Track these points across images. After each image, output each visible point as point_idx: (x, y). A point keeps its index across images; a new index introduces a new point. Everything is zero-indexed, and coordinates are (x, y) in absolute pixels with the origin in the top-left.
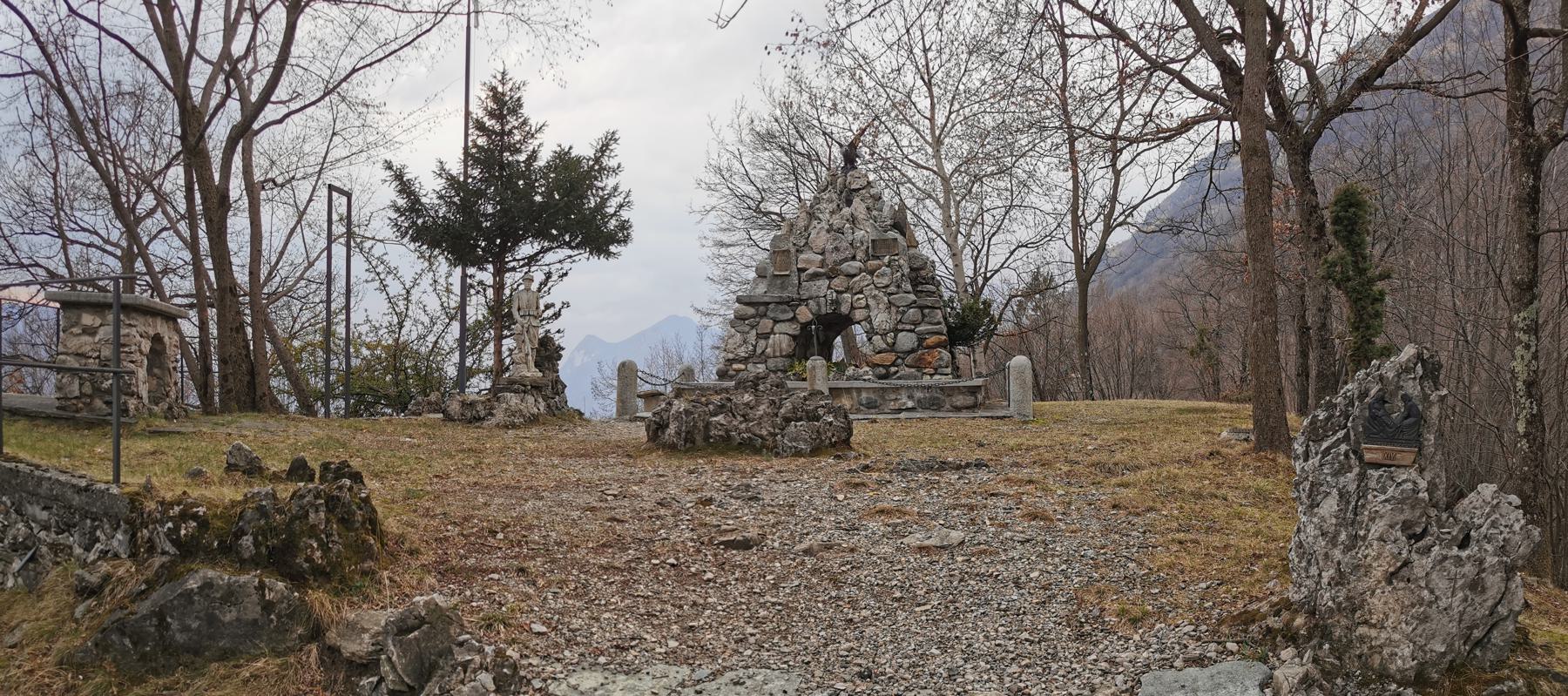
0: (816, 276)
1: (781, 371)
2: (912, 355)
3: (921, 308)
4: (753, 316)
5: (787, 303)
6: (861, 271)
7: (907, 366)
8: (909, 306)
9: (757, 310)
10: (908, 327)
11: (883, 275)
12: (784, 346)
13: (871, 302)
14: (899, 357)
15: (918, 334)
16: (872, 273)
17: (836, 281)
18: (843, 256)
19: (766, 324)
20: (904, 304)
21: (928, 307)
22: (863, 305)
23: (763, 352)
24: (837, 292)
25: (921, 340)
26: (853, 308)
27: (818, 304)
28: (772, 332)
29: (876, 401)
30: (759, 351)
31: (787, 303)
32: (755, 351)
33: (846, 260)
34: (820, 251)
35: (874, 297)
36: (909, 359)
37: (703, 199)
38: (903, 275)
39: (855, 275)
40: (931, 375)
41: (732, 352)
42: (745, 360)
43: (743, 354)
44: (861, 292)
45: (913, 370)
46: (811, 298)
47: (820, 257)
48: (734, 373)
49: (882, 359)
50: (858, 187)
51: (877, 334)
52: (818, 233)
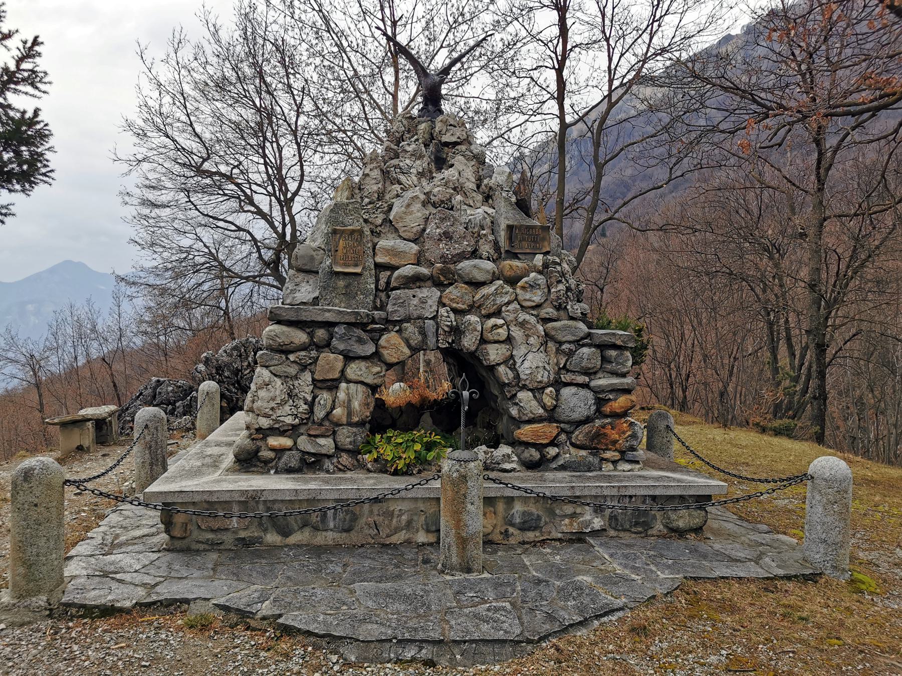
0: (415, 281)
1: (348, 451)
2: (586, 428)
3: (602, 347)
4: (304, 348)
5: (363, 326)
6: (495, 277)
7: (574, 445)
8: (578, 343)
9: (311, 335)
10: (581, 379)
11: (532, 286)
12: (356, 405)
13: (517, 333)
14: (563, 430)
15: (596, 391)
16: (512, 281)
17: (454, 292)
18: (457, 249)
19: (329, 363)
20: (570, 338)
21: (614, 347)
22: (504, 338)
23: (328, 414)
24: (455, 311)
25: (600, 402)
26: (483, 341)
27: (423, 332)
28: (343, 377)
29: (539, 518)
30: (319, 413)
31: (363, 326)
32: (311, 411)
33: (462, 256)
34: (411, 235)
35: (522, 325)
36: (579, 435)
37: (129, 145)
38: (568, 289)
39: (483, 284)
40: (614, 462)
41: (267, 416)
42: (292, 431)
43: (289, 420)
44: (497, 313)
45: (583, 453)
46: (408, 319)
47: (415, 248)
48: (271, 455)
49: (535, 432)
50: (454, 139)
51: (524, 387)
52: (408, 206)
